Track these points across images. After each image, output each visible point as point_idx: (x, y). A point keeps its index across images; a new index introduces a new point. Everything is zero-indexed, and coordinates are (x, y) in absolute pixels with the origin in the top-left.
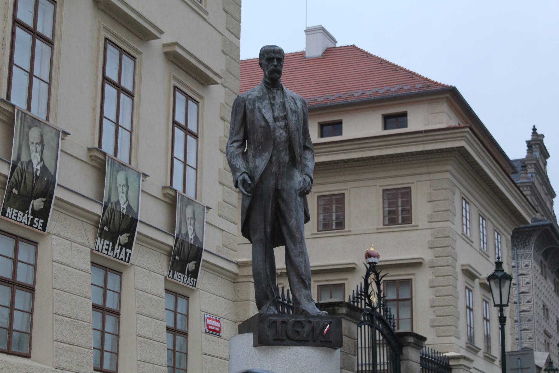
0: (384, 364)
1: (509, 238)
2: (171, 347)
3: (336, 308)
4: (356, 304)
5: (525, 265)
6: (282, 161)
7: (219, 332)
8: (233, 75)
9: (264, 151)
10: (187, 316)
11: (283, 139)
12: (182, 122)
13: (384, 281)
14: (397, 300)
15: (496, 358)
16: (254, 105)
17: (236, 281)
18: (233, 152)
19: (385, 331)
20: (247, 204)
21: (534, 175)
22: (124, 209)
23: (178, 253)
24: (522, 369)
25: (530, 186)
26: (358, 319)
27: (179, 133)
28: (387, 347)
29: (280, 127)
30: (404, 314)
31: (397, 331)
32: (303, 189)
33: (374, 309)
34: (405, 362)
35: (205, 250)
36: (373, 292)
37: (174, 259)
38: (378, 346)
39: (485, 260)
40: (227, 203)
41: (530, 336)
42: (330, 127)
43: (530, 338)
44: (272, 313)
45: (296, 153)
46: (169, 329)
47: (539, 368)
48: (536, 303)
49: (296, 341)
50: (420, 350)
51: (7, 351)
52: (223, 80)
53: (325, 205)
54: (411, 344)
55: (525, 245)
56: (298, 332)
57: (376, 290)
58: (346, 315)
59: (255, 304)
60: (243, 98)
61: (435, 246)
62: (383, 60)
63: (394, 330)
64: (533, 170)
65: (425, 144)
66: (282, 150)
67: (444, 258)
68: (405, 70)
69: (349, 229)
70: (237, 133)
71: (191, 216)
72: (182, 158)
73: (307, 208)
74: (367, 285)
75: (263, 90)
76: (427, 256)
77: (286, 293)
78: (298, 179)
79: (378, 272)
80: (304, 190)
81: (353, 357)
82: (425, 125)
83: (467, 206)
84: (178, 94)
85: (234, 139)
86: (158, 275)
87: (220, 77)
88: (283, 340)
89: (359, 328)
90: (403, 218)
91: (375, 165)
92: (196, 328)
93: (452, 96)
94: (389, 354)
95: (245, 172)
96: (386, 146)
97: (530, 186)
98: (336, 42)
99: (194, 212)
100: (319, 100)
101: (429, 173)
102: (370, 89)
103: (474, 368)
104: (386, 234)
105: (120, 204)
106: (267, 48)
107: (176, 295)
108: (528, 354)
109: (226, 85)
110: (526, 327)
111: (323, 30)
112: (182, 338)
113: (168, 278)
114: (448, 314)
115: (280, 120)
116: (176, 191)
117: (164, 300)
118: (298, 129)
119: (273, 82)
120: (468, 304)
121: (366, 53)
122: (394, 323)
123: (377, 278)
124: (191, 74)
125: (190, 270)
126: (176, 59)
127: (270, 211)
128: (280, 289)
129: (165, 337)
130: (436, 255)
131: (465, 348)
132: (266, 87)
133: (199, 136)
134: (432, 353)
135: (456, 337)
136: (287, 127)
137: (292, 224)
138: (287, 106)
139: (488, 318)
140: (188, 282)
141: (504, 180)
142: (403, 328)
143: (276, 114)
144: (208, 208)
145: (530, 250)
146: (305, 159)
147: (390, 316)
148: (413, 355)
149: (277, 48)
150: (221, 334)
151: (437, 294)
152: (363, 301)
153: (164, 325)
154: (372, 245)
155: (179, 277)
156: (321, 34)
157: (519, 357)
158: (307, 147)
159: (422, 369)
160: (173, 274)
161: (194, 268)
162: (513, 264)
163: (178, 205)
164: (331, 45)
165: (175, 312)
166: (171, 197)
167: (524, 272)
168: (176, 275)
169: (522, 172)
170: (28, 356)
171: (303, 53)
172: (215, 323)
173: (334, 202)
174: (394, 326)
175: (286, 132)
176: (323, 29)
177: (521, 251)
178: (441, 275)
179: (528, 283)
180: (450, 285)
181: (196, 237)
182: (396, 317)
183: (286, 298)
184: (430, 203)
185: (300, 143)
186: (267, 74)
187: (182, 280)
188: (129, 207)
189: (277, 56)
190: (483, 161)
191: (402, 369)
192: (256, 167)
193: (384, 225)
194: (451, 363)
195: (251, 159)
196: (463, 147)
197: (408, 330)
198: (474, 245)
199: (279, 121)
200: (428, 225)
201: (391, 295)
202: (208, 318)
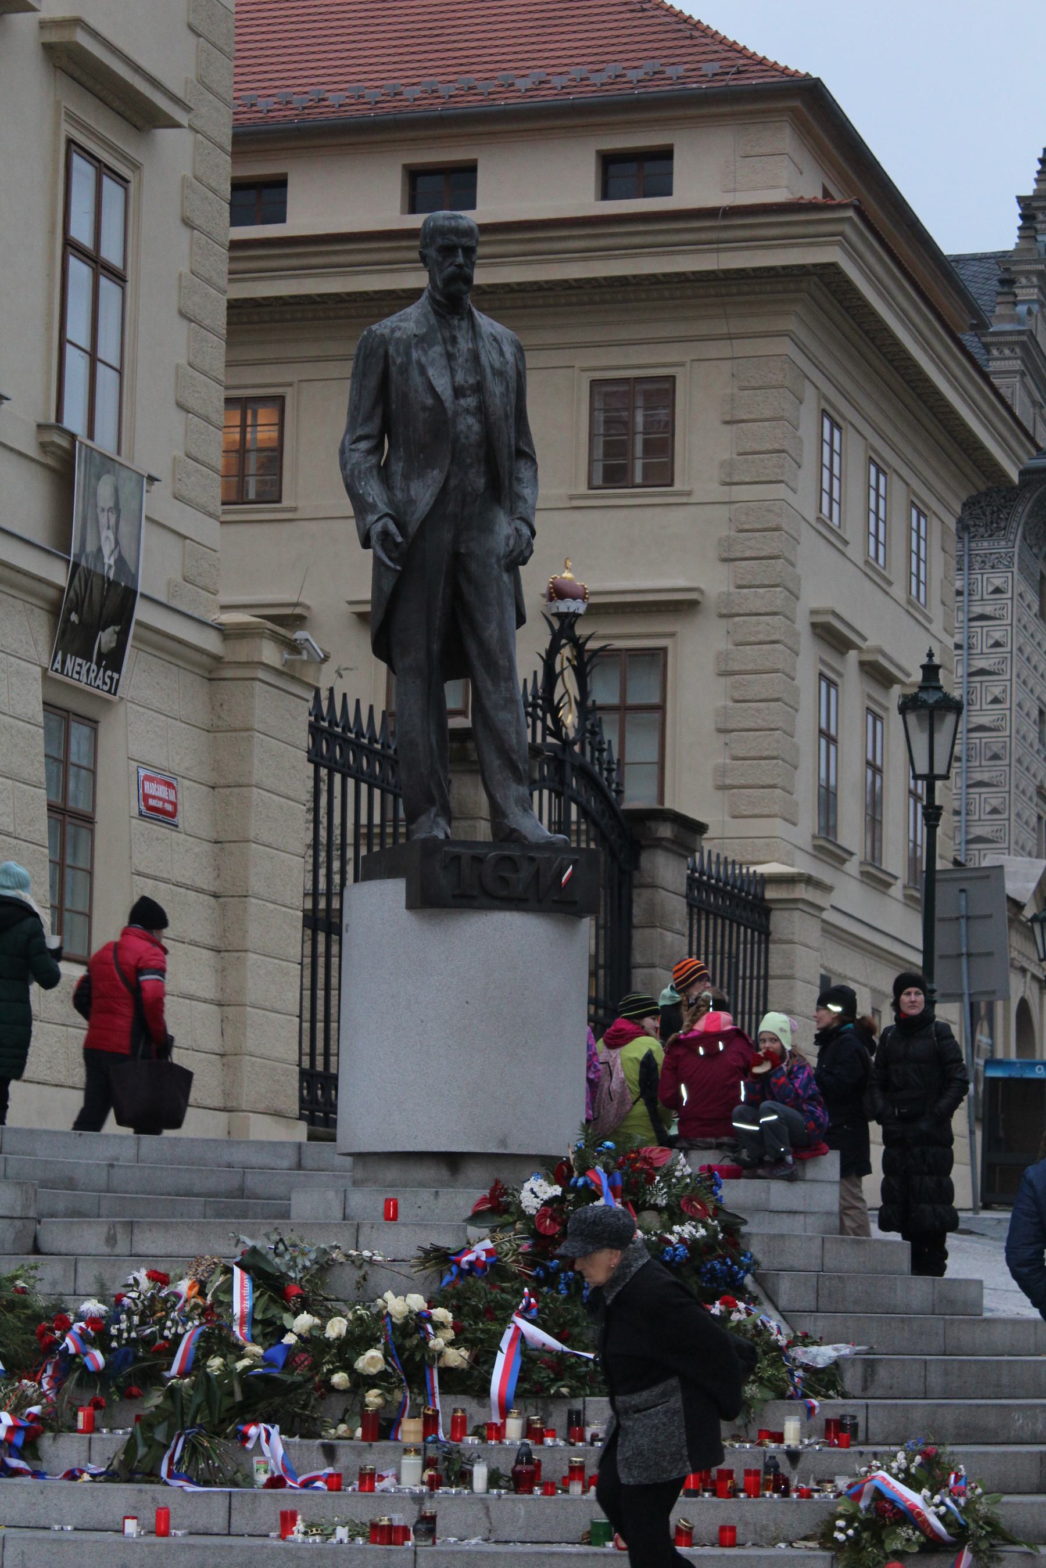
1: (952, 524)
5: (991, 589)
6: (470, 489)
7: (173, 815)
11: (474, 438)
14: (623, 709)
15: (896, 878)
16: (408, 355)
17: (214, 675)
18: (358, 463)
20: (388, 585)
21: (1035, 308)
23: (76, 606)
24: (968, 918)
25: (1023, 345)
27: (80, 271)
30: (640, 749)
31: (625, 806)
32: (515, 554)
33: (567, 744)
34: (646, 893)
35: (143, 596)
36: (566, 699)
37: (67, 620)
39: (880, 595)
40: (196, 460)
41: (995, 802)
43: (995, 811)
47: (1017, 906)
48: (1019, 761)
49: (502, 899)
54: (664, 843)
55: (995, 527)
56: (503, 879)
57: (574, 691)
60: (383, 335)
61: (739, 555)
64: (1034, 294)
67: (761, 590)
70: (368, 418)
71: (110, 504)
72: (85, 342)
73: (522, 600)
74: (551, 677)
76: (712, 581)
83: (836, 433)
84: (77, 161)
85: (360, 432)
87: (187, 108)
88: (474, 897)
90: (645, 466)
91: (571, 304)
92: (115, 802)
93: (807, 107)
95: (387, 515)
97: (1023, 345)
101: (730, 337)
103: (832, 906)
104: (596, 514)
108: (988, 877)
110: (985, 777)
113: (50, 673)
114: (766, 754)
115: (468, 392)
116: (73, 437)
120: (823, 725)
125: (104, 650)
130: (739, 582)
131: (810, 849)
132: (436, 312)
133: (129, 277)
134: (718, 863)
135: (785, 819)
136: (482, 411)
138: (484, 359)
139: (878, 762)
140: (99, 682)
141: (946, 358)
142: (637, 796)
143: (460, 378)
144: (152, 479)
145: (1011, 544)
146: (519, 480)
148: (668, 873)
150: (179, 819)
151: (737, 696)
152: (539, 724)
154: (569, 564)
155: (77, 668)
157: (964, 885)
160: (64, 662)
161: (113, 645)
162: (958, 584)
167: (988, 610)
168: (69, 664)
169: (1000, 299)
172: (162, 791)
175: (480, 422)
177: (984, 546)
178: (752, 639)
179: (997, 644)
180: (777, 671)
181: (120, 561)
184: (728, 427)
185: (510, 446)
189: (464, 241)
190: (889, 306)
191: (636, 910)
192: (411, 502)
193: (591, 487)
194: (770, 894)
195: (398, 480)
196: (834, 265)
198: (849, 551)
199: (464, 396)
200: (721, 493)
202: (151, 779)
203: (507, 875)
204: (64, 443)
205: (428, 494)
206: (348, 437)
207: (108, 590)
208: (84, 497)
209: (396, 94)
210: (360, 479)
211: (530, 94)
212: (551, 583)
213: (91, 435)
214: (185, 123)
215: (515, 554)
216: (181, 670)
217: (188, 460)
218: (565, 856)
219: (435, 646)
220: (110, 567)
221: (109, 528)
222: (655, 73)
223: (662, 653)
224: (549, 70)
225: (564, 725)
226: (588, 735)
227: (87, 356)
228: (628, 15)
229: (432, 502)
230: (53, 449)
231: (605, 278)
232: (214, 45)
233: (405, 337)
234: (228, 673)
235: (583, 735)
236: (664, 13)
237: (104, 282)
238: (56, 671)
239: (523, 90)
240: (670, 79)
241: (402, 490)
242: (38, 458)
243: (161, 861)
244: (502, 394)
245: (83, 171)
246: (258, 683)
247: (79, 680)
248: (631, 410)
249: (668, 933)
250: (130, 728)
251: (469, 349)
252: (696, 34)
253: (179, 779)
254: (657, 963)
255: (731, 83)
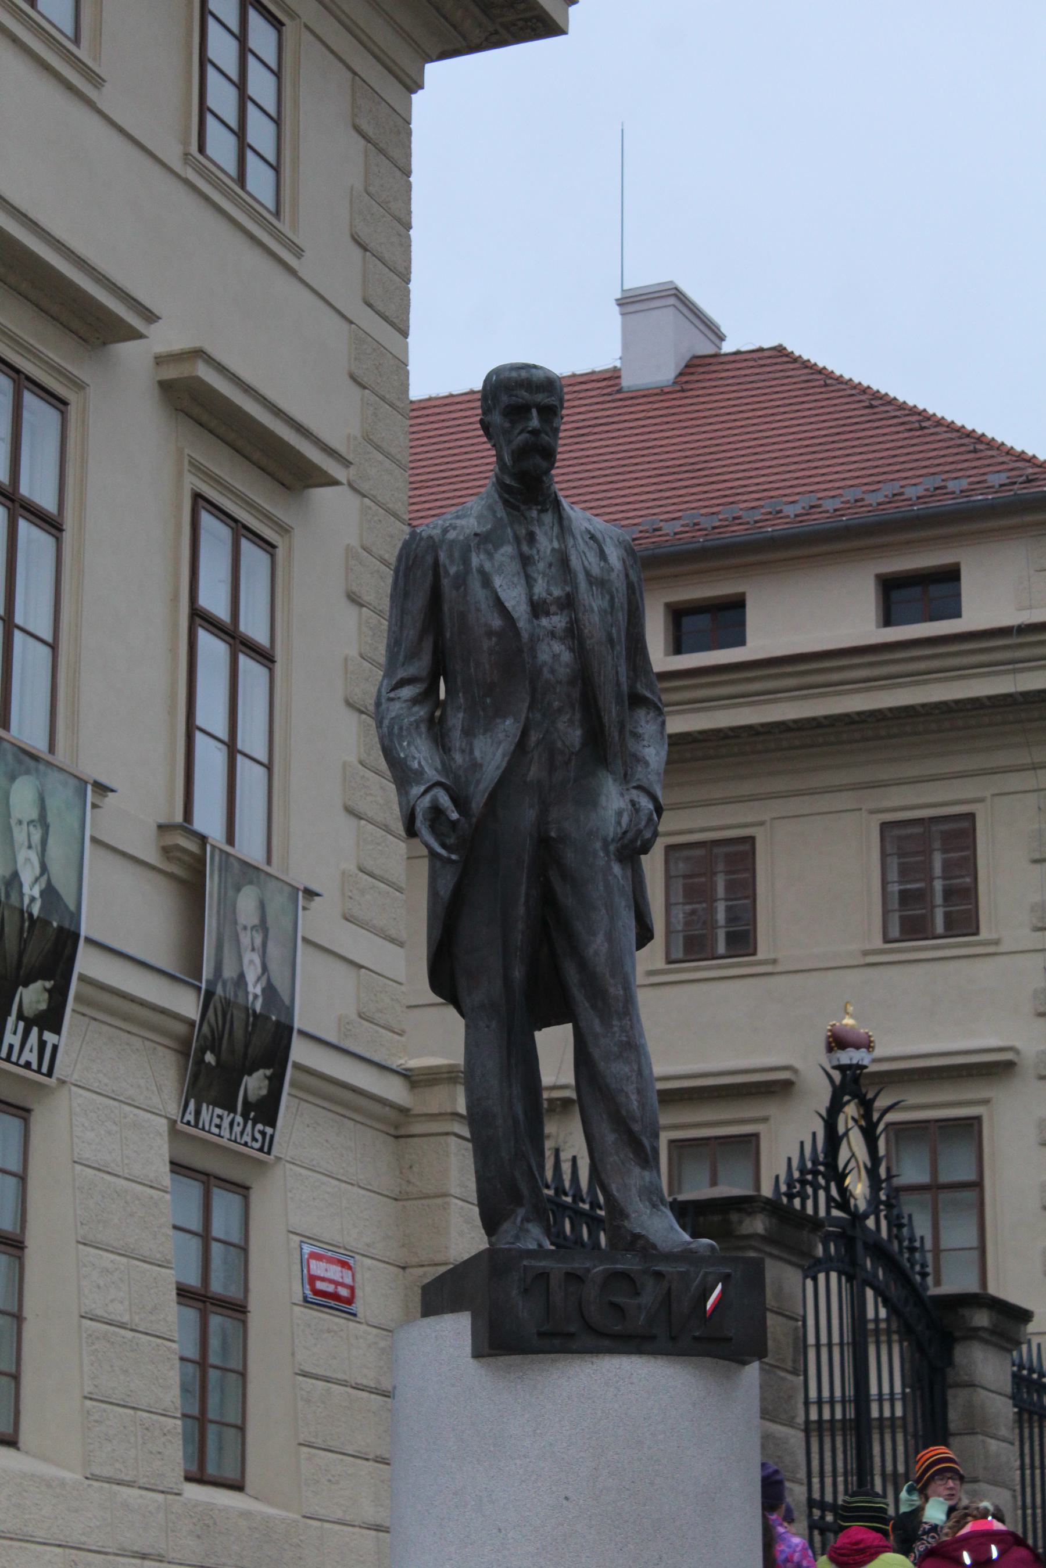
0: (892, 1400)
2: (193, 1353)
3: (734, 1217)
4: (797, 1202)
6: (559, 744)
7: (350, 1301)
8: (388, 455)
9: (499, 712)
10: (244, 1249)
11: (563, 672)
12: (221, 611)
13: (888, 1125)
14: (934, 1188)
16: (466, 561)
18: (397, 717)
19: (894, 1291)
20: (447, 884)
22: (33, 899)
23: (213, 1043)
26: (808, 1254)
27: (212, 649)
28: (901, 1343)
29: (552, 634)
30: (957, 1234)
31: (933, 1291)
32: (629, 835)
33: (857, 1218)
36: (853, 1164)
37: (200, 1061)
38: (871, 1339)
42: (703, 621)
44: (532, 1246)
45: (606, 720)
46: (184, 1294)
50: (1010, 1351)
51: (198, 1476)
52: (352, 470)
53: (691, 876)
54: (982, 1334)
57: (862, 1154)
58: (767, 1239)
59: (476, 1210)
60: (430, 537)
62: (877, 395)
63: (926, 1288)
65: (1022, 670)
66: (560, 710)
68: (951, 427)
69: (772, 956)
70: (412, 656)
72: (221, 730)
74: (834, 1140)
75: (494, 512)
77: (566, 1167)
78: (614, 803)
79: (870, 1096)
80: (633, 841)
81: (790, 1377)
82: (1021, 609)
84: (207, 520)
85: (401, 674)
86: (149, 1115)
87: (346, 463)
88: (571, 1336)
89: (809, 1283)
90: (947, 915)
92: (273, 1287)
94: (907, 1366)
96: (891, 681)
98: (722, 338)
99: (262, 906)
100: (668, 528)
102: (839, 490)
105: (21, 885)
106: (507, 374)
107: (208, 1181)
109: (365, 487)
111: (677, 296)
112: (229, 1324)
113: (180, 1126)
115: (553, 609)
116: (203, 839)
117: (168, 1197)
118: (611, 641)
119: (526, 485)
121: (822, 371)
122: (924, 1265)
123: (867, 1114)
124: (244, 452)
126: (196, 403)
127: (521, 910)
128: (549, 1154)
129: (173, 1318)
132: (506, 503)
136: (574, 634)
137: (596, 953)
138: (575, 562)
140: (247, 1138)
142: (956, 1280)
143: (540, 589)
144: (310, 894)
147: (912, 1239)
148: (988, 1369)
149: (540, 374)
150: (358, 1306)
152: (822, 1194)
153: (169, 1279)
154: (850, 1009)
155: (217, 1121)
156: (672, 309)
158: (642, 694)
159: (1020, 1414)
160: (198, 1113)
161: (264, 1092)
163: (212, 884)
164: (706, 348)
165: (205, 1237)
166: (186, 858)
168: (205, 1115)
170: (238, 1487)
171: (612, 376)
172: (334, 1272)
173: (721, 867)
174: (924, 1275)
175: (571, 650)
176: (678, 295)
181: (270, 991)
182: (928, 1245)
183: (567, 1184)
184: (1038, 866)
185: (618, 684)
186: (507, 458)
187: (226, 1133)
188: (50, 893)
189: (540, 398)
192: (475, 766)
193: (886, 941)
195: (456, 738)
197: (968, 1284)
199: (547, 614)
201: (912, 1171)
202: (313, 1256)
203: (619, 1300)
204: (192, 846)
205: (500, 752)
206: (385, 681)
207: (254, 1025)
208: (218, 912)
209: (655, 530)
210: (401, 737)
211: (800, 519)
212: (830, 1031)
213: (230, 840)
214: (344, 481)
215: (629, 835)
216: (359, 1126)
217: (361, 874)
218: (711, 1269)
219: (517, 973)
220: (256, 996)
221: (253, 950)
222: (936, 488)
223: (975, 1122)
224: (820, 495)
225: (851, 1195)
226: (882, 1207)
227: (224, 748)
228: (906, 435)
229: (504, 764)
230: (179, 854)
231: (891, 709)
232: (383, 399)
233: (461, 537)
234: (418, 1128)
235: (877, 1207)
236: (945, 429)
237: (245, 662)
238: (188, 1123)
239: (792, 516)
240: (953, 493)
241: (463, 751)
242: (159, 865)
243: (335, 1358)
244: (603, 612)
245: (215, 534)
246: (454, 1138)
247: (219, 1136)
248: (928, 853)
249: (993, 1442)
250: (290, 1195)
251: (553, 550)
252: (979, 447)
253: (357, 1257)
254: (980, 1478)
255: (1019, 492)
